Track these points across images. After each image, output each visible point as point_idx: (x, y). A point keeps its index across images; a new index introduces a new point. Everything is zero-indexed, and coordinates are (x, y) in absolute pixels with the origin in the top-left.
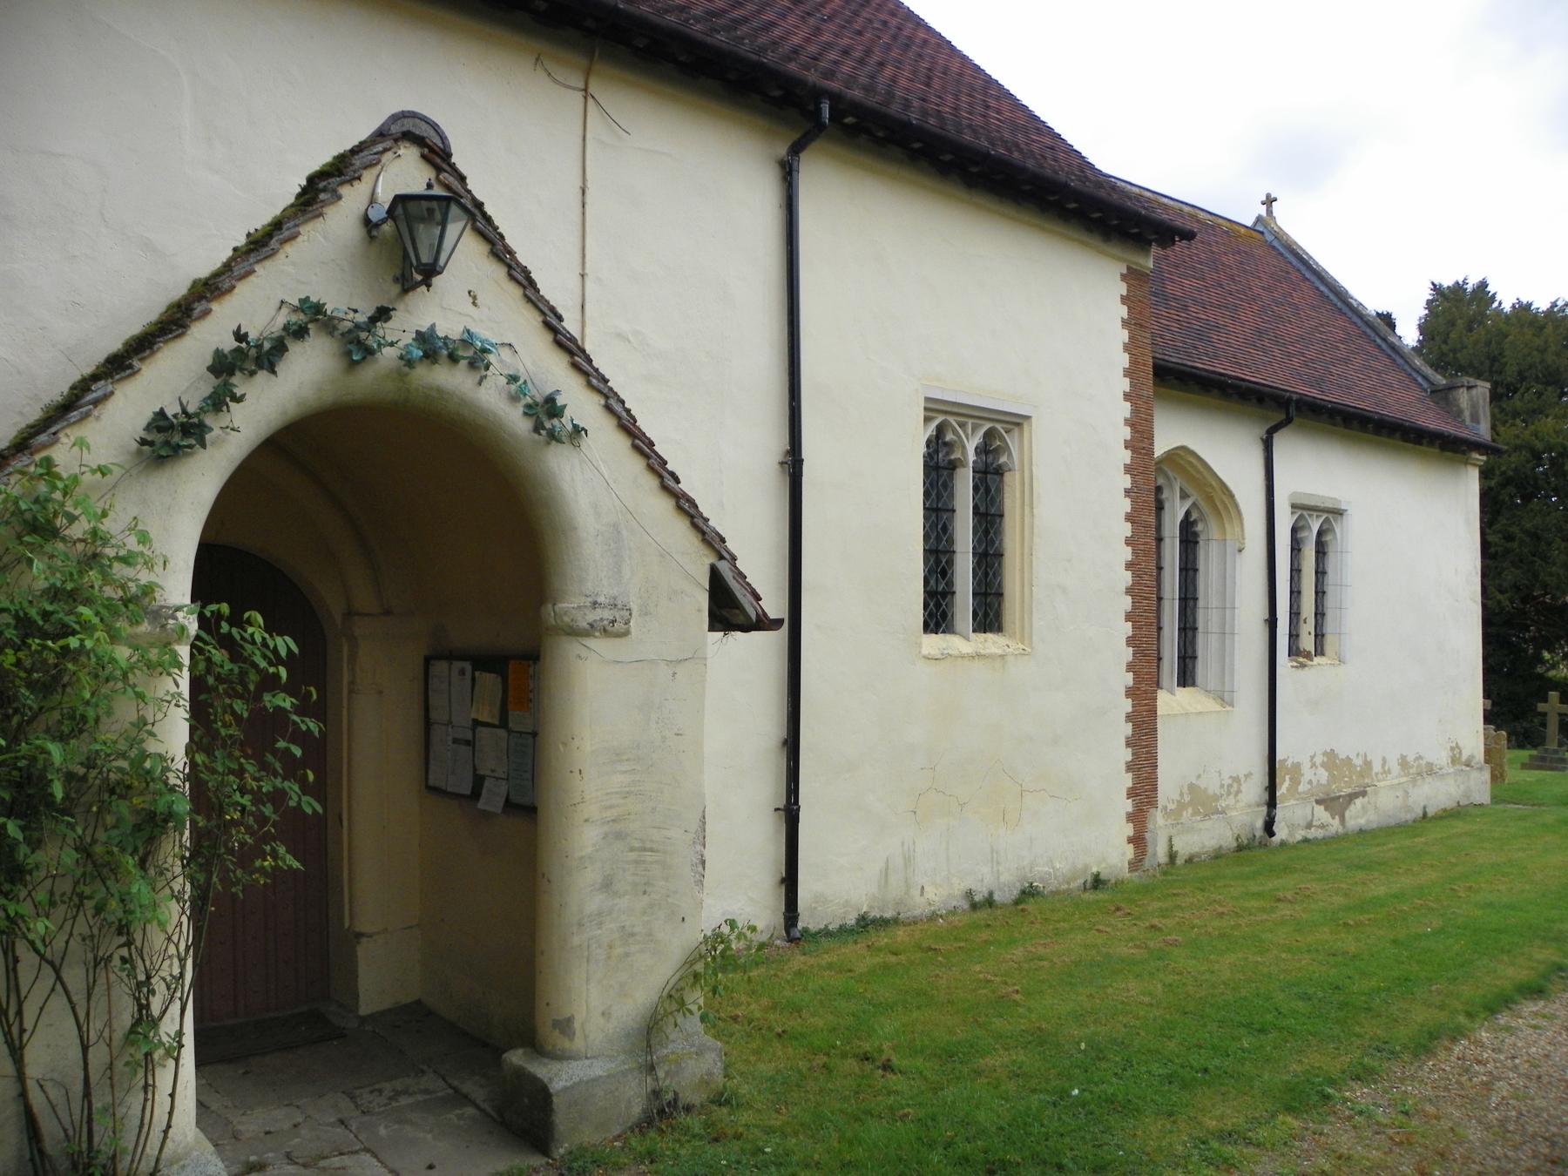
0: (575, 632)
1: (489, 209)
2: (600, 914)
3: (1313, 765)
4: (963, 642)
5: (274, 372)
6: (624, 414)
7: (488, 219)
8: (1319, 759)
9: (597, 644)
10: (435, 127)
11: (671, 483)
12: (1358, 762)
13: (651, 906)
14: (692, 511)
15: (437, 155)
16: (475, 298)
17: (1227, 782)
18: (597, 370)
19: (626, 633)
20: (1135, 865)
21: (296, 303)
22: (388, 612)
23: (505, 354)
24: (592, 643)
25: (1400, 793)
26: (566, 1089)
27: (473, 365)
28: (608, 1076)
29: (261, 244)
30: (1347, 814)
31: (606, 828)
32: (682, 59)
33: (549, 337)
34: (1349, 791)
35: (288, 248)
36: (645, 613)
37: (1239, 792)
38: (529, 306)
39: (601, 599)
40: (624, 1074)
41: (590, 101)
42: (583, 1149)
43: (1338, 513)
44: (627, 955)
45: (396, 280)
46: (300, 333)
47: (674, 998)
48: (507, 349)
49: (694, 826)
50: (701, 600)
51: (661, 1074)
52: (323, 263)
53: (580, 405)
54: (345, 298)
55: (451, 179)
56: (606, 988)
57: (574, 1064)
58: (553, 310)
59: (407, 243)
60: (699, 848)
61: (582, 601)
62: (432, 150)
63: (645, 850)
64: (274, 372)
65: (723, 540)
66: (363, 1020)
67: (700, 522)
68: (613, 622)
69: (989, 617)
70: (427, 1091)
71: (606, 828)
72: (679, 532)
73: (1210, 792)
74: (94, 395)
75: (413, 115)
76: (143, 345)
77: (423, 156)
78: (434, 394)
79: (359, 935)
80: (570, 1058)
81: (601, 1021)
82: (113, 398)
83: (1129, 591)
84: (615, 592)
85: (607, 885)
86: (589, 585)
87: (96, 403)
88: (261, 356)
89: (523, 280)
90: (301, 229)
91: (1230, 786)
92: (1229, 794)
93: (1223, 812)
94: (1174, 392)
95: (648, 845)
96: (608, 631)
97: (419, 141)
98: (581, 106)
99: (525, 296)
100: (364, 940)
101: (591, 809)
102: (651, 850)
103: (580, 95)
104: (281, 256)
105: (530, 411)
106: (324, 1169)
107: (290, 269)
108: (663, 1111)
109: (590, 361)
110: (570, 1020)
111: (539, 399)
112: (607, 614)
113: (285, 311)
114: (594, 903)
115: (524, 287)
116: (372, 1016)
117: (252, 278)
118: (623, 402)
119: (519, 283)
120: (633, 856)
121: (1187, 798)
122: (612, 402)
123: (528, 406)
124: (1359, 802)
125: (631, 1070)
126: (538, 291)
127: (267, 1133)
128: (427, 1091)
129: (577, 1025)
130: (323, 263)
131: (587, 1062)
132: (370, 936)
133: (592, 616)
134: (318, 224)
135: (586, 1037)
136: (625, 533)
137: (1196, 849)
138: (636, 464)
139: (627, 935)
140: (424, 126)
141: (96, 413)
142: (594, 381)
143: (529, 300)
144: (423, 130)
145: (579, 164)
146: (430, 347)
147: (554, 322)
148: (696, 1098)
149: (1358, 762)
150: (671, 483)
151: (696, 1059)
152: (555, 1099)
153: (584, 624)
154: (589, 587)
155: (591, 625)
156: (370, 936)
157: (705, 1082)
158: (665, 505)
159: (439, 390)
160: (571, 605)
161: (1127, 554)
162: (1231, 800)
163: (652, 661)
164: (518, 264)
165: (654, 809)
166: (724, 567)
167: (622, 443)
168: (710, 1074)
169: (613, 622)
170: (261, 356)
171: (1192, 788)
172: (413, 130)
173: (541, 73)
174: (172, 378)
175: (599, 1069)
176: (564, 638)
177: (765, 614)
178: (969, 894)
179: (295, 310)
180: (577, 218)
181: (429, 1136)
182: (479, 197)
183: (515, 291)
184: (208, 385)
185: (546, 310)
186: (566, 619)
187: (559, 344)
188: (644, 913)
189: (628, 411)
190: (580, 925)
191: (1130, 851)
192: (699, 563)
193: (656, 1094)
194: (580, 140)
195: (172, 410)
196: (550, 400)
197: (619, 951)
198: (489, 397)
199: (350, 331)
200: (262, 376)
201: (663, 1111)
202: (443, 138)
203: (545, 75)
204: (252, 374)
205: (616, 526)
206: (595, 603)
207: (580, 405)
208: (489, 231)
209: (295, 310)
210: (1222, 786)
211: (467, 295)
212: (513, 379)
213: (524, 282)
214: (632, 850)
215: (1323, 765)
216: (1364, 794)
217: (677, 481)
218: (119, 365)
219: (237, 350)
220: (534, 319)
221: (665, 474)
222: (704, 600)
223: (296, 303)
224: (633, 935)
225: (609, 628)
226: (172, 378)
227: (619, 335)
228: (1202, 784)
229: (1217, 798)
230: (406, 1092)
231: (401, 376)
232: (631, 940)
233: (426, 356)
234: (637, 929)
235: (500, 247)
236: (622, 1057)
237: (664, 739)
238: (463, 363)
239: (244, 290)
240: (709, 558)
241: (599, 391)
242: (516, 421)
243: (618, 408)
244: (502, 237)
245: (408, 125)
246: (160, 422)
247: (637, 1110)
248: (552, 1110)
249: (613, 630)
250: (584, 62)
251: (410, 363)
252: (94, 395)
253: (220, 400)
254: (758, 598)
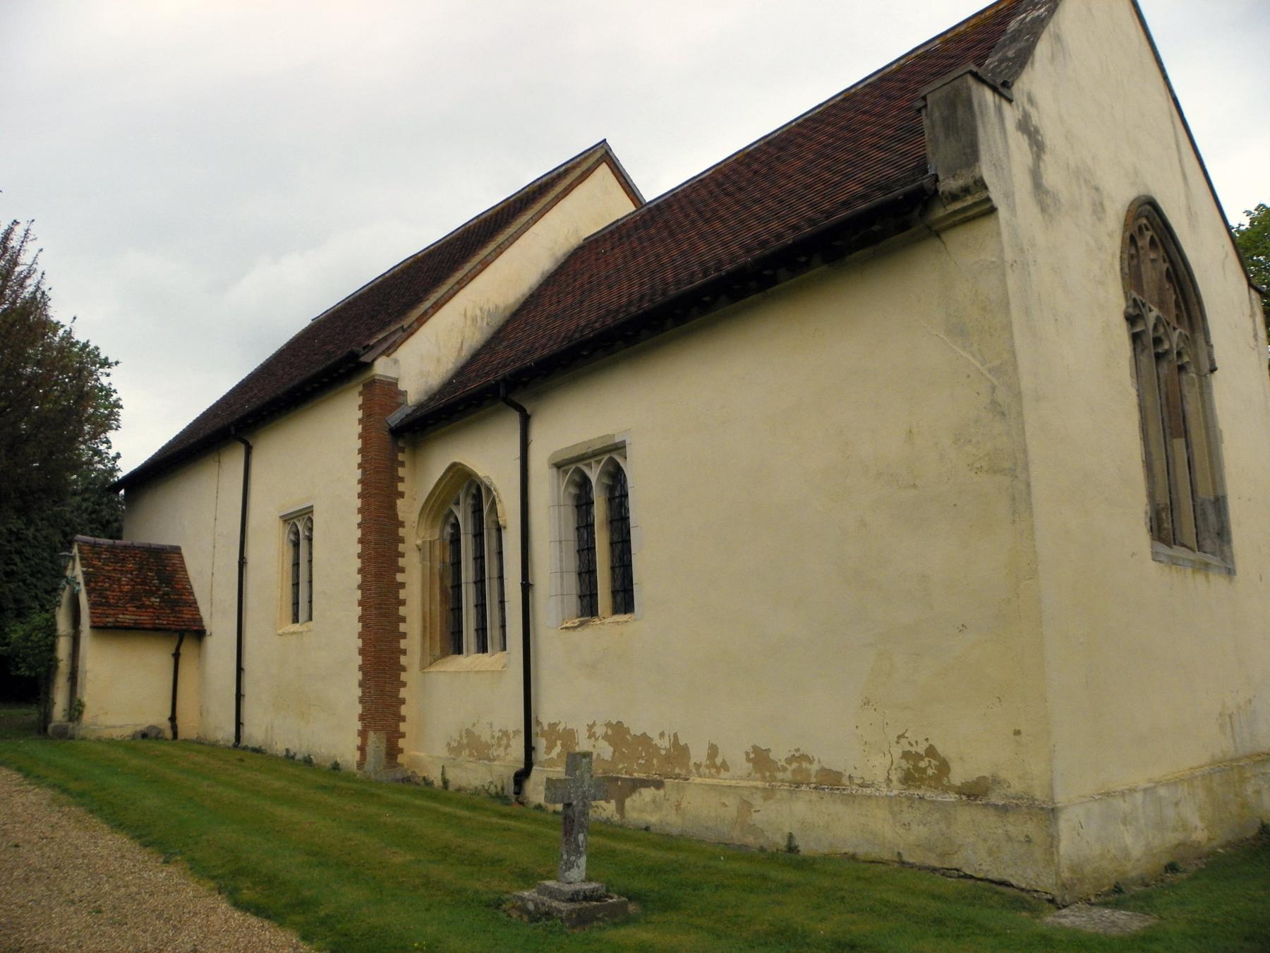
3: (592, 735)
4: (608, 625)
8: (600, 730)
12: (664, 744)
17: (497, 734)
20: (361, 764)
25: (732, 802)
30: (628, 802)
34: (642, 776)
37: (507, 746)
43: (620, 448)
69: (624, 600)
73: (483, 739)
83: (360, 587)
91: (500, 739)
92: (499, 746)
93: (490, 760)
94: (443, 429)
121: (465, 741)
124: (648, 794)
137: (464, 784)
149: (664, 744)
161: (358, 563)
162: (501, 752)
171: (469, 733)
178: (287, 750)
191: (357, 755)
210: (493, 737)
215: (606, 737)
216: (659, 785)
228: (477, 731)
229: (489, 747)
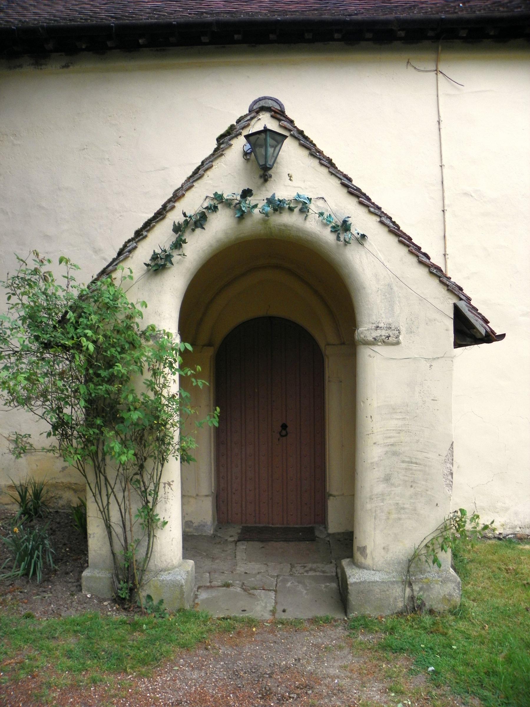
0: (367, 343)
1: (306, 133)
2: (383, 494)
5: (204, 228)
6: (391, 224)
7: (306, 138)
9: (380, 349)
10: (276, 101)
11: (424, 259)
13: (416, 494)
14: (439, 274)
15: (278, 114)
16: (291, 177)
18: (373, 204)
19: (398, 343)
21: (213, 196)
22: (343, 344)
23: (320, 203)
24: (376, 348)
26: (355, 583)
27: (302, 211)
28: (383, 582)
29: (197, 174)
31: (387, 449)
32: (492, 33)
33: (345, 191)
35: (209, 173)
36: (410, 331)
38: (333, 177)
39: (381, 325)
40: (393, 583)
41: (440, 75)
42: (364, 617)
44: (400, 519)
45: (261, 177)
46: (214, 209)
47: (430, 548)
48: (321, 201)
49: (445, 453)
50: (448, 325)
51: (416, 588)
52: (229, 176)
53: (362, 221)
54: (231, 189)
55: (286, 123)
56: (388, 536)
57: (366, 571)
58: (346, 176)
59: (261, 156)
60: (449, 465)
61: (370, 326)
62: (275, 112)
63: (412, 463)
64: (204, 228)
65: (461, 289)
66: (329, 535)
67: (445, 280)
68: (388, 337)
70: (324, 572)
71: (387, 449)
72: (432, 288)
74: (129, 248)
75: (265, 98)
76: (149, 225)
77: (272, 116)
78: (283, 228)
79: (331, 495)
80: (364, 568)
81: (383, 552)
82: (138, 249)
84: (390, 321)
85: (387, 479)
86: (374, 317)
87: (130, 252)
88: (200, 221)
89: (328, 164)
90: (214, 164)
95: (414, 460)
96: (386, 342)
97: (268, 109)
98: (435, 79)
99: (330, 172)
100: (331, 498)
101: (378, 437)
102: (416, 463)
103: (433, 74)
104: (206, 176)
105: (335, 230)
106: (250, 594)
107: (210, 182)
108: (415, 607)
109: (369, 199)
110: (365, 548)
111: (339, 224)
112: (384, 333)
113: (207, 200)
114: (380, 488)
115: (329, 168)
116: (334, 534)
117: (193, 189)
118: (390, 218)
119: (326, 166)
120: (404, 465)
122: (383, 219)
123: (333, 227)
125: (397, 582)
126: (337, 168)
127: (246, 573)
128: (324, 572)
129: (368, 551)
130: (229, 176)
131: (373, 572)
132: (334, 496)
133: (375, 334)
134: (223, 159)
135: (373, 559)
136: (395, 289)
138: (403, 251)
139: (400, 509)
140: (270, 102)
141: (131, 256)
142: (372, 209)
143: (332, 174)
144: (270, 104)
145: (436, 109)
146: (277, 206)
147: (346, 182)
148: (439, 607)
150: (424, 259)
151: (443, 585)
152: (349, 587)
153: (370, 339)
154: (374, 318)
155: (375, 339)
156: (334, 496)
157: (447, 599)
158: (423, 272)
159: (285, 225)
160: (365, 330)
163: (415, 358)
164: (324, 157)
165: (418, 441)
166: (462, 305)
167: (393, 240)
168: (450, 595)
169: (388, 337)
170: (200, 221)
172: (265, 105)
173: (410, 68)
174: (161, 237)
175: (377, 577)
176: (362, 346)
177: (492, 331)
179: (213, 199)
180: (437, 138)
181: (305, 592)
182: (301, 128)
183: (324, 171)
184: (173, 237)
185: (341, 177)
186: (362, 336)
187: (350, 193)
188: (411, 498)
189: (394, 223)
190: (371, 499)
192: (446, 304)
193: (412, 598)
194: (436, 97)
195: (158, 251)
196: (345, 222)
197: (394, 516)
198: (312, 226)
199: (237, 204)
200: (198, 231)
201: (415, 607)
202: (281, 105)
203: (413, 69)
204: (193, 230)
205: (390, 286)
206: (378, 327)
207: (362, 221)
208: (308, 144)
209: (213, 199)
211: (295, 176)
212: (321, 214)
213: (329, 165)
214: (403, 462)
217: (428, 258)
218: (140, 235)
219: (186, 220)
220: (335, 183)
221: (420, 254)
222: (450, 324)
223: (213, 196)
224: (403, 508)
225: (386, 340)
226: (161, 237)
227: (466, 194)
230: (315, 570)
231: (265, 222)
232: (402, 511)
233: (275, 210)
234: (405, 506)
235: (313, 150)
236: (394, 574)
237: (424, 402)
238: (296, 210)
239: (189, 195)
240: (452, 300)
241: (376, 214)
242: (327, 236)
243: (387, 222)
244: (315, 145)
245: (262, 103)
246: (155, 257)
247: (400, 605)
248: (348, 593)
249: (390, 340)
250: (434, 56)
251: (267, 215)
252: (129, 248)
253: (178, 244)
254: (487, 322)
